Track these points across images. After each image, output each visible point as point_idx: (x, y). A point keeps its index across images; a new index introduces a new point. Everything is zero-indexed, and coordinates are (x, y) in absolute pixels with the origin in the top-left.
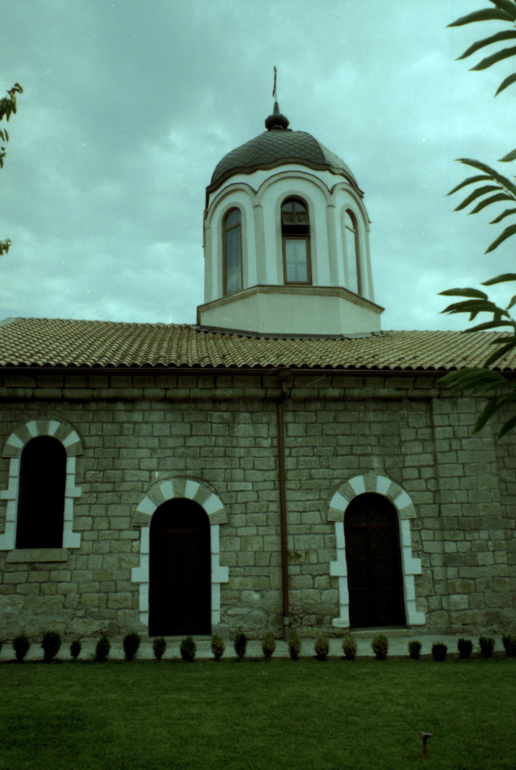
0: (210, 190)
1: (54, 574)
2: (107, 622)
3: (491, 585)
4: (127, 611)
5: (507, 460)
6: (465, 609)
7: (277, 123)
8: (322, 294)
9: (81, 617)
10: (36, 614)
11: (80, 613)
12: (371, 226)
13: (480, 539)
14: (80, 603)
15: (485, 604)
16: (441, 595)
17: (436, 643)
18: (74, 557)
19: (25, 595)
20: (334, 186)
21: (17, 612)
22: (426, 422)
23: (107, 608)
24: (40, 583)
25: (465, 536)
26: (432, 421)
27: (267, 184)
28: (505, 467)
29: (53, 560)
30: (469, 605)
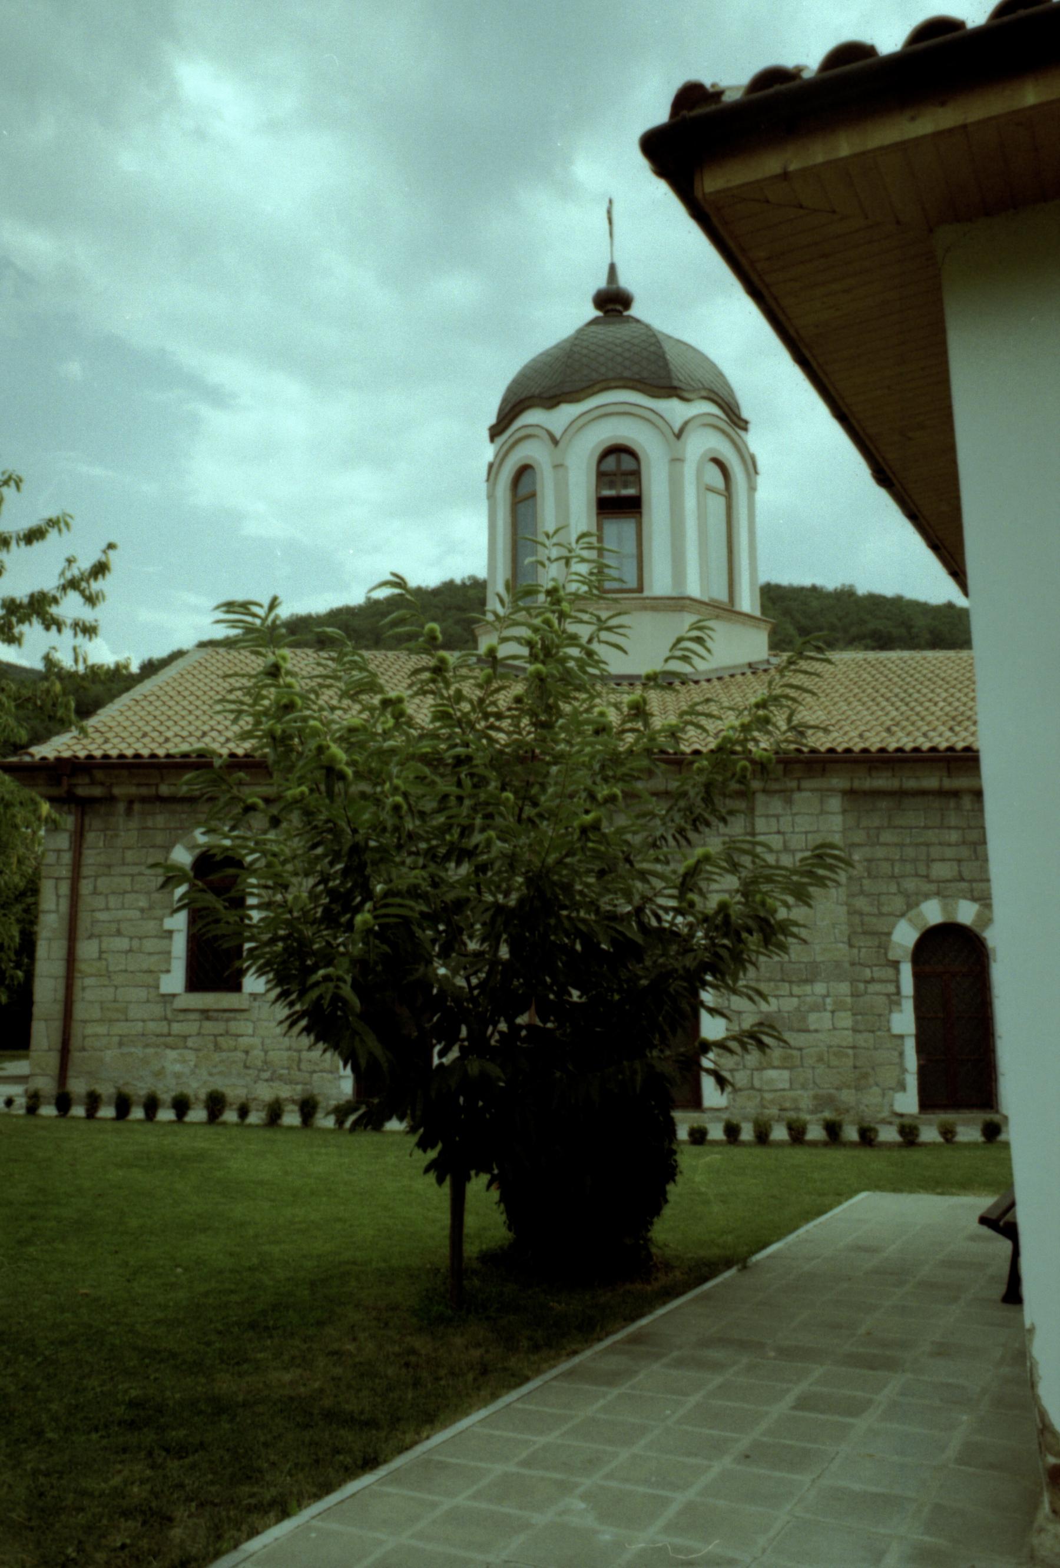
0: (495, 432)
1: (232, 1024)
2: (299, 1087)
3: (826, 1058)
4: (325, 1074)
5: (865, 882)
6: (784, 1090)
7: (613, 302)
8: (654, 609)
9: (267, 1080)
10: (211, 1074)
11: (266, 1075)
12: (761, 481)
13: (813, 994)
14: (265, 1062)
15: (814, 1083)
16: (753, 1070)
17: (695, 1125)
18: (256, 1004)
19: (197, 1050)
20: (686, 423)
21: (187, 1071)
22: (745, 827)
23: (299, 1070)
24: (215, 1036)
25: (791, 990)
26: (753, 825)
27: (576, 426)
28: (862, 892)
29: (232, 1007)
30: (791, 1084)
